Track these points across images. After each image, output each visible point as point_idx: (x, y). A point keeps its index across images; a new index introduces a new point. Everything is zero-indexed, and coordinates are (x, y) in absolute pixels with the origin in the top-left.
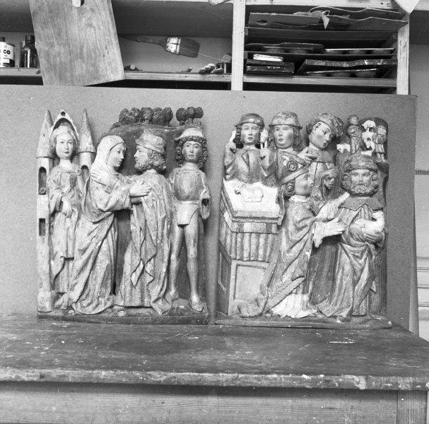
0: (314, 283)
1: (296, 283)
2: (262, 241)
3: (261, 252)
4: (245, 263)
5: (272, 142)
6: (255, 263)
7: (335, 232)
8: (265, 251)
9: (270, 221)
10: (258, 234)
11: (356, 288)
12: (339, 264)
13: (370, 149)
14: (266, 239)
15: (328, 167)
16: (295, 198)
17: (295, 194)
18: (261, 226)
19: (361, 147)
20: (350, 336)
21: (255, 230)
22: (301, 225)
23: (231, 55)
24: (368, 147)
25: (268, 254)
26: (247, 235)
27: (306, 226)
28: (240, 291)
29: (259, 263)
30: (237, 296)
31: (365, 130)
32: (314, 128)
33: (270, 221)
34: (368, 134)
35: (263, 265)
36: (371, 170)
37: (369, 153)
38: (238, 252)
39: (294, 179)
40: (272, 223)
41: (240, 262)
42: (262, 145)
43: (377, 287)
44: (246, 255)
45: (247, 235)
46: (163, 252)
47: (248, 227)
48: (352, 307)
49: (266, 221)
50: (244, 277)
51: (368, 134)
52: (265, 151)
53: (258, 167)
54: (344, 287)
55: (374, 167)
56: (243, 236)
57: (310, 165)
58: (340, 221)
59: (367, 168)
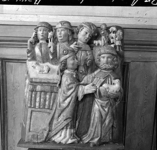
0: (79, 122)
1: (66, 123)
2: (48, 96)
3: (47, 103)
4: (37, 110)
5: (55, 38)
6: (43, 110)
7: (90, 92)
8: (50, 103)
9: (53, 85)
10: (46, 93)
11: (103, 125)
12: (93, 111)
13: (113, 43)
14: (50, 96)
15: (88, 54)
16: (67, 71)
17: (67, 69)
18: (47, 88)
19: (108, 42)
20: (89, 60)
21: (43, 89)
22: (70, 87)
23: (40, 4)
24: (112, 42)
25: (51, 104)
26: (38, 93)
27: (72, 88)
28: (33, 126)
29: (45, 109)
30: (31, 130)
31: (111, 33)
32: (80, 30)
33: (53, 85)
34: (112, 35)
35: (48, 111)
36: (113, 55)
37: (113, 46)
38: (33, 103)
39: (66, 59)
40: (54, 86)
41: (33, 109)
42: (49, 40)
43: (116, 125)
44: (37, 104)
45: (38, 93)
46: (111, 95)
47: (39, 88)
48: (101, 138)
49: (51, 85)
50: (36, 118)
51: (112, 35)
52: (50, 44)
53: (47, 54)
54: (95, 125)
55: (115, 53)
56: (36, 94)
57: (77, 52)
58: (93, 85)
59: (110, 53)
